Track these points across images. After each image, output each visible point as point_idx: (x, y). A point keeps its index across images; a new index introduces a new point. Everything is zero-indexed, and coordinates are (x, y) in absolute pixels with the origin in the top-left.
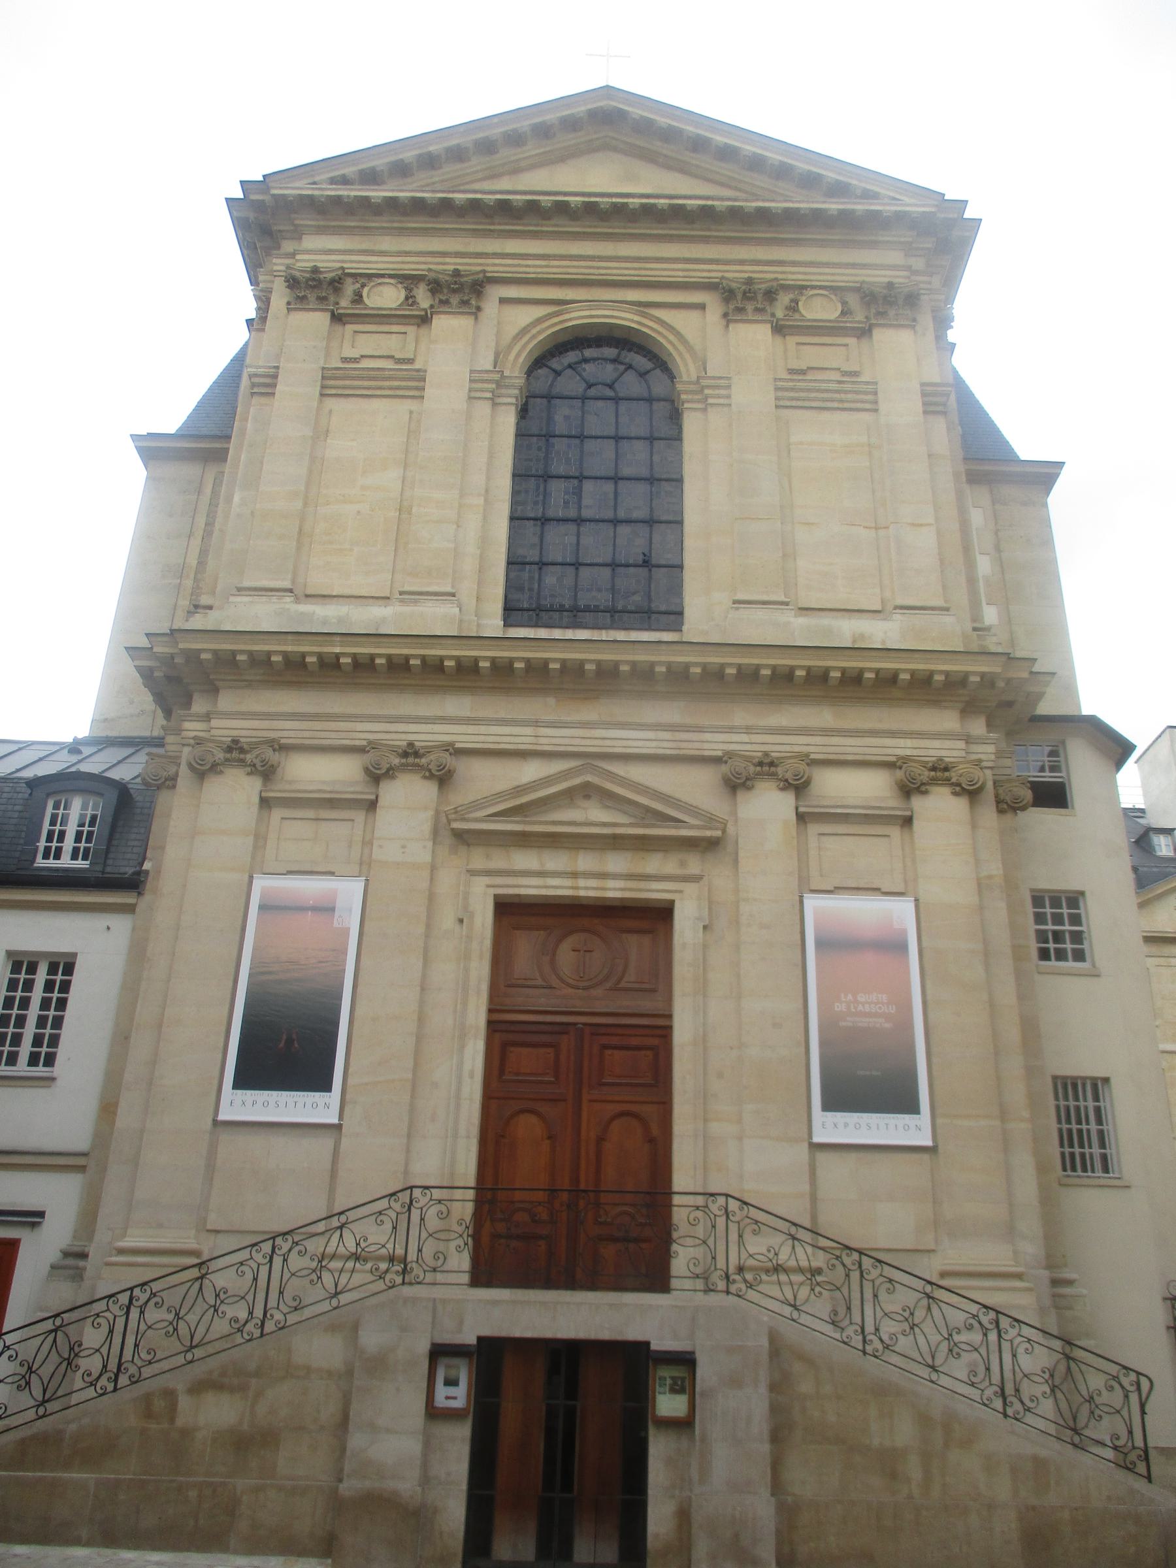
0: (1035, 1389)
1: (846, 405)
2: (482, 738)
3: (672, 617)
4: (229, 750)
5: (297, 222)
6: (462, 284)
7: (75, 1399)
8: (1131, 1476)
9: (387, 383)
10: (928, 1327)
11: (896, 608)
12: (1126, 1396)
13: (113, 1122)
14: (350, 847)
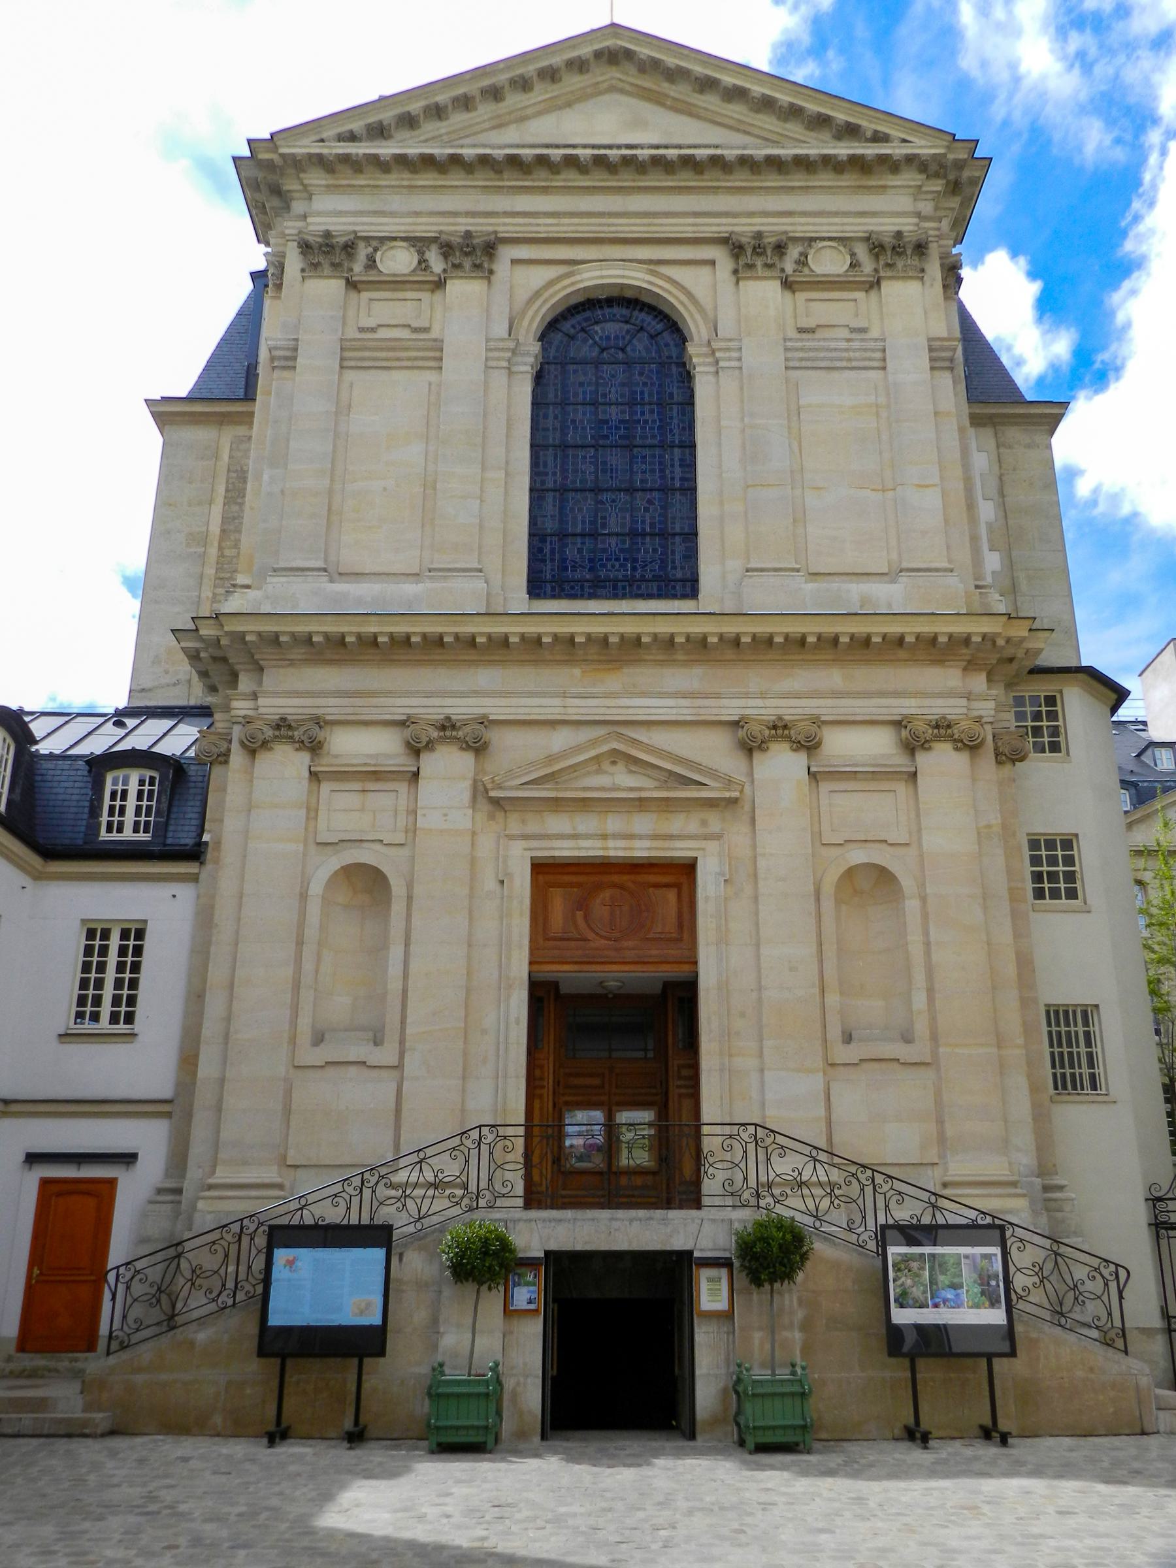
1: (854, 364)
2: (513, 710)
4: (278, 727)
5: (306, 182)
8: (1111, 1350)
12: (1106, 1285)
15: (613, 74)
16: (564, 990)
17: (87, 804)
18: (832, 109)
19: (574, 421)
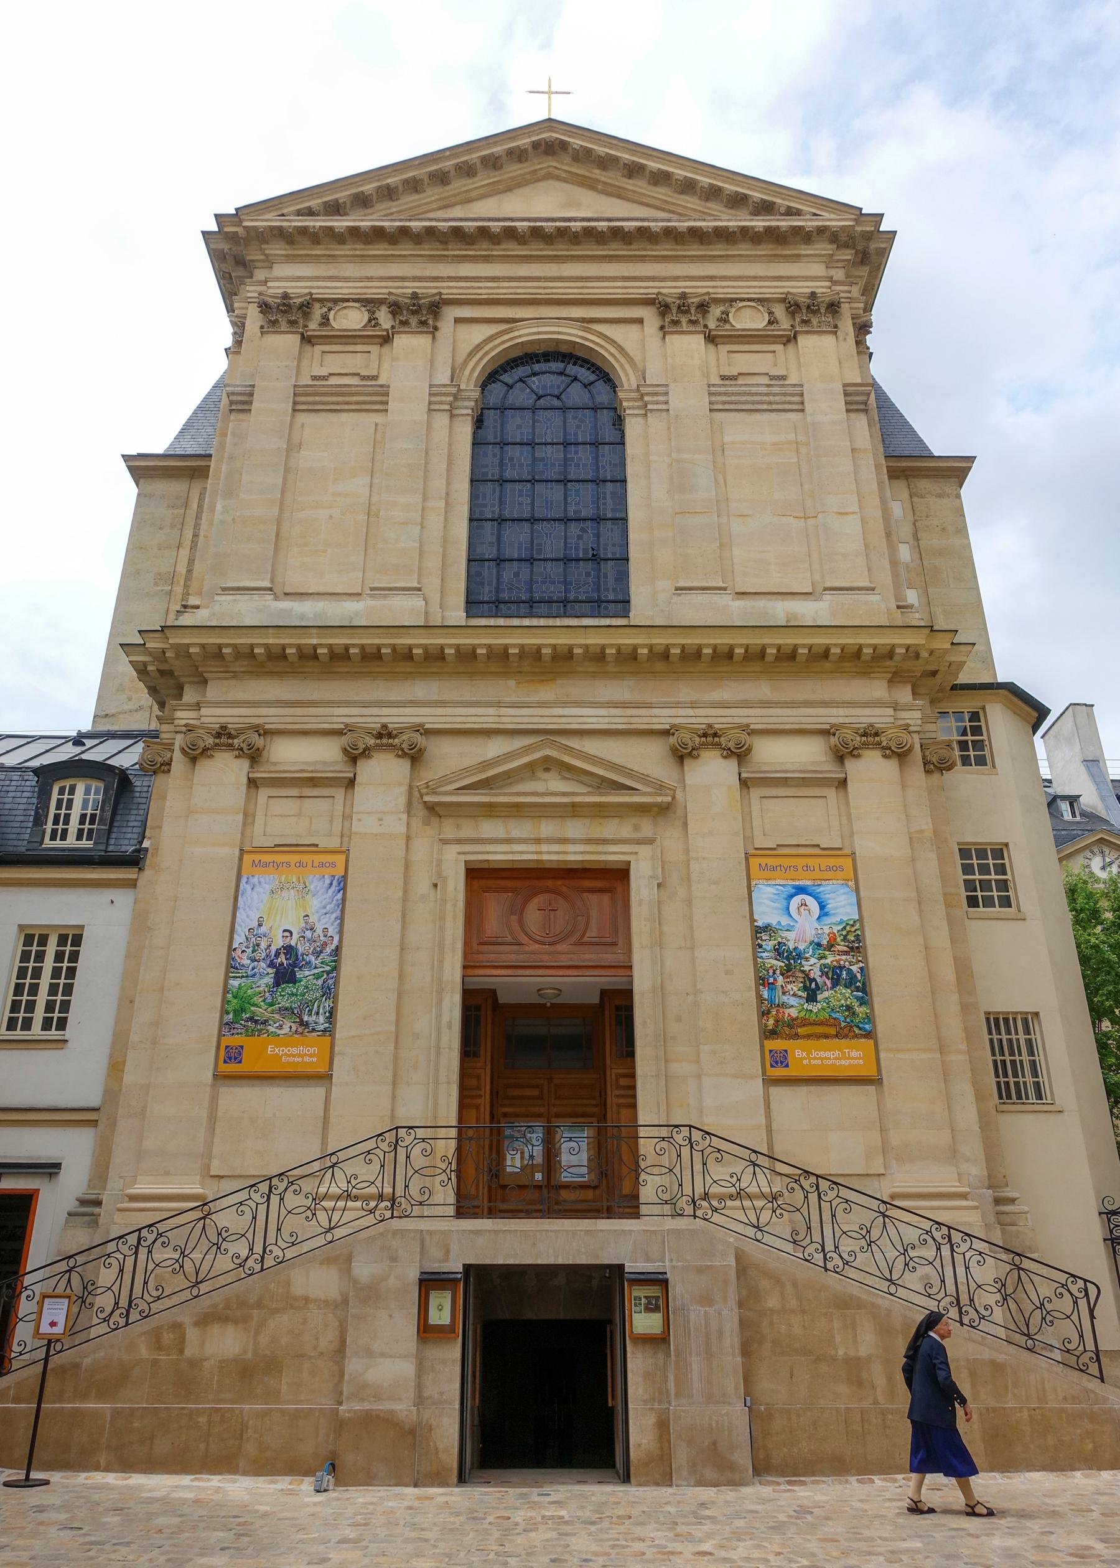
0: (990, 1298)
1: (774, 407)
2: (449, 719)
3: (620, 605)
4: (218, 735)
5: (267, 252)
6: (420, 306)
7: (94, 1333)
9: (354, 399)
10: (884, 1242)
11: (825, 589)
12: (1075, 1303)
13: (122, 1079)
14: (331, 821)
15: (550, 162)
16: (502, 1000)
17: (33, 813)
18: (749, 188)
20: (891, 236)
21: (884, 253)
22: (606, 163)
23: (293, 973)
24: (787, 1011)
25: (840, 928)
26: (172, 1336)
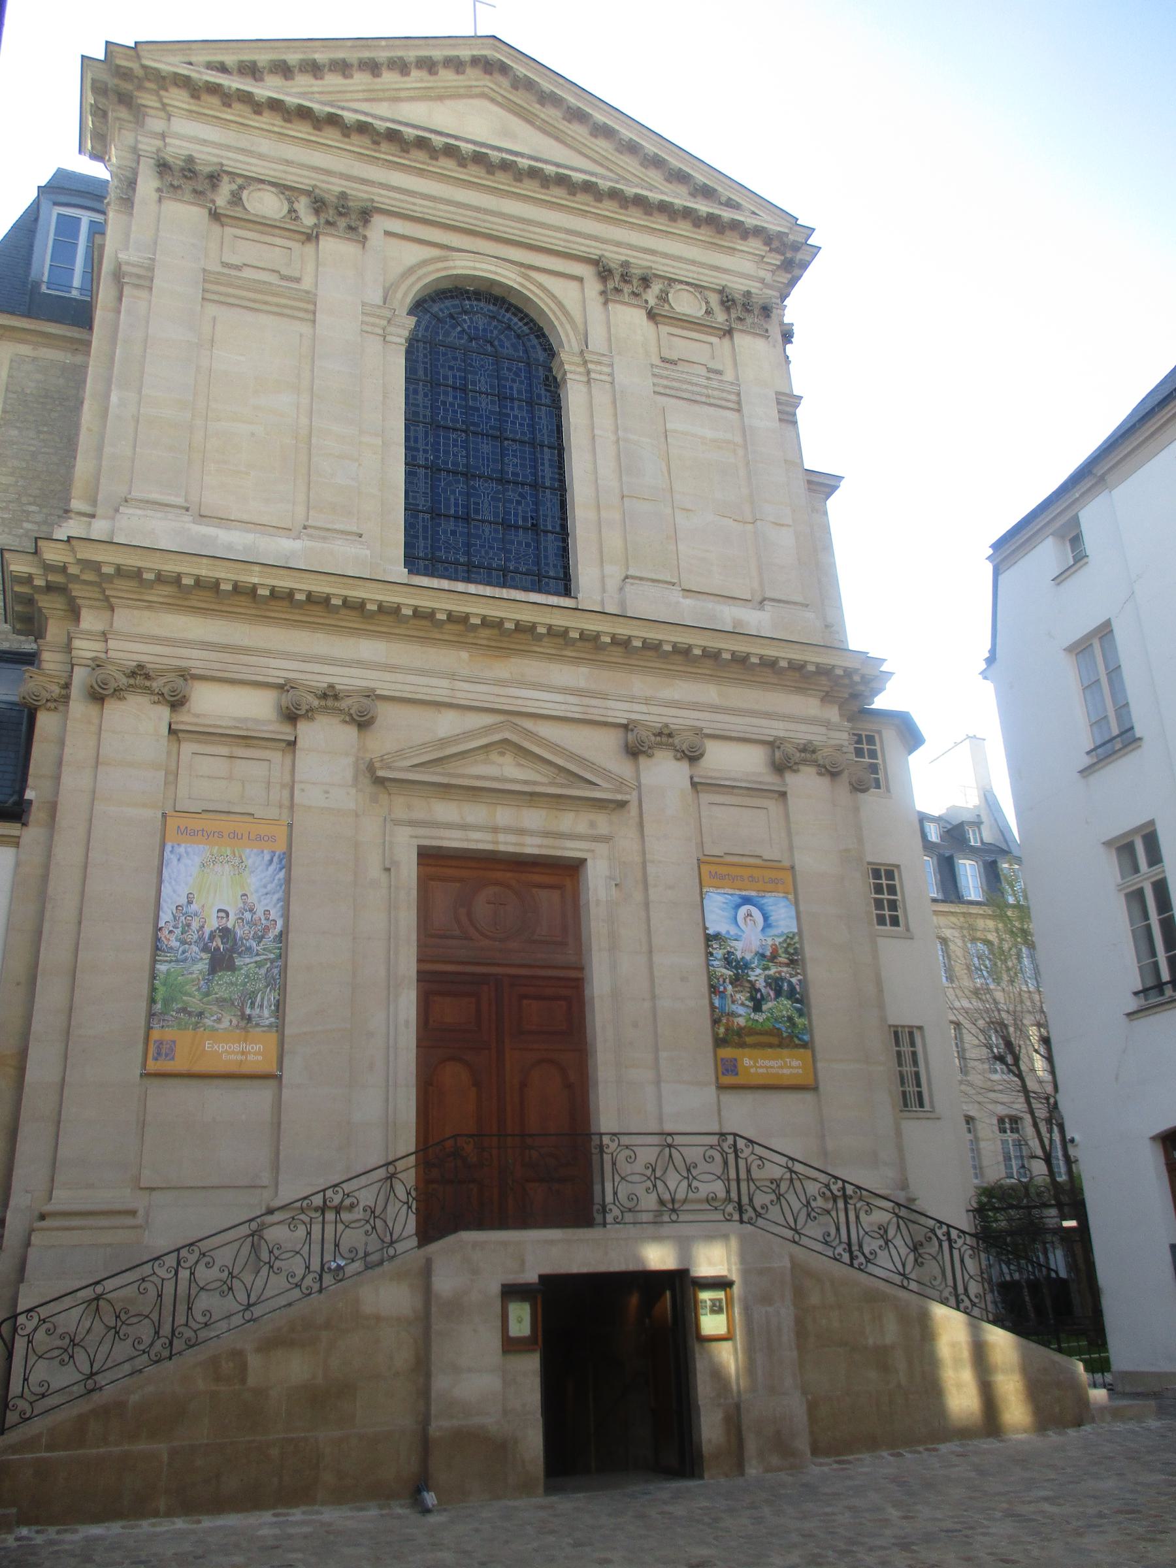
1: (712, 401)
4: (133, 674)
5: (166, 101)
18: (692, 168)
19: (444, 403)
20: (815, 250)
21: (804, 266)
22: (548, 99)
23: (231, 959)
24: (736, 1020)
25: (781, 940)
26: (231, 1365)
